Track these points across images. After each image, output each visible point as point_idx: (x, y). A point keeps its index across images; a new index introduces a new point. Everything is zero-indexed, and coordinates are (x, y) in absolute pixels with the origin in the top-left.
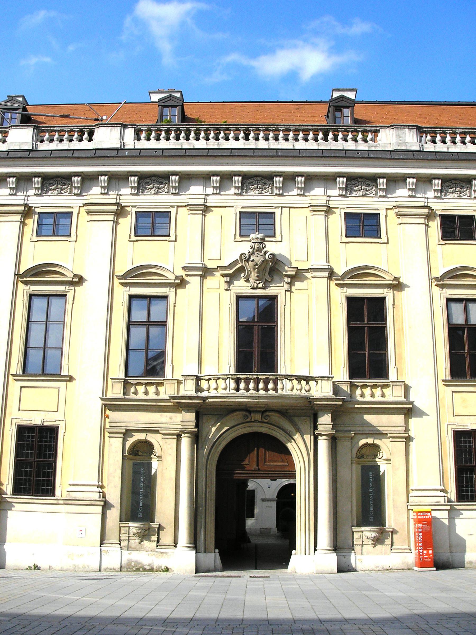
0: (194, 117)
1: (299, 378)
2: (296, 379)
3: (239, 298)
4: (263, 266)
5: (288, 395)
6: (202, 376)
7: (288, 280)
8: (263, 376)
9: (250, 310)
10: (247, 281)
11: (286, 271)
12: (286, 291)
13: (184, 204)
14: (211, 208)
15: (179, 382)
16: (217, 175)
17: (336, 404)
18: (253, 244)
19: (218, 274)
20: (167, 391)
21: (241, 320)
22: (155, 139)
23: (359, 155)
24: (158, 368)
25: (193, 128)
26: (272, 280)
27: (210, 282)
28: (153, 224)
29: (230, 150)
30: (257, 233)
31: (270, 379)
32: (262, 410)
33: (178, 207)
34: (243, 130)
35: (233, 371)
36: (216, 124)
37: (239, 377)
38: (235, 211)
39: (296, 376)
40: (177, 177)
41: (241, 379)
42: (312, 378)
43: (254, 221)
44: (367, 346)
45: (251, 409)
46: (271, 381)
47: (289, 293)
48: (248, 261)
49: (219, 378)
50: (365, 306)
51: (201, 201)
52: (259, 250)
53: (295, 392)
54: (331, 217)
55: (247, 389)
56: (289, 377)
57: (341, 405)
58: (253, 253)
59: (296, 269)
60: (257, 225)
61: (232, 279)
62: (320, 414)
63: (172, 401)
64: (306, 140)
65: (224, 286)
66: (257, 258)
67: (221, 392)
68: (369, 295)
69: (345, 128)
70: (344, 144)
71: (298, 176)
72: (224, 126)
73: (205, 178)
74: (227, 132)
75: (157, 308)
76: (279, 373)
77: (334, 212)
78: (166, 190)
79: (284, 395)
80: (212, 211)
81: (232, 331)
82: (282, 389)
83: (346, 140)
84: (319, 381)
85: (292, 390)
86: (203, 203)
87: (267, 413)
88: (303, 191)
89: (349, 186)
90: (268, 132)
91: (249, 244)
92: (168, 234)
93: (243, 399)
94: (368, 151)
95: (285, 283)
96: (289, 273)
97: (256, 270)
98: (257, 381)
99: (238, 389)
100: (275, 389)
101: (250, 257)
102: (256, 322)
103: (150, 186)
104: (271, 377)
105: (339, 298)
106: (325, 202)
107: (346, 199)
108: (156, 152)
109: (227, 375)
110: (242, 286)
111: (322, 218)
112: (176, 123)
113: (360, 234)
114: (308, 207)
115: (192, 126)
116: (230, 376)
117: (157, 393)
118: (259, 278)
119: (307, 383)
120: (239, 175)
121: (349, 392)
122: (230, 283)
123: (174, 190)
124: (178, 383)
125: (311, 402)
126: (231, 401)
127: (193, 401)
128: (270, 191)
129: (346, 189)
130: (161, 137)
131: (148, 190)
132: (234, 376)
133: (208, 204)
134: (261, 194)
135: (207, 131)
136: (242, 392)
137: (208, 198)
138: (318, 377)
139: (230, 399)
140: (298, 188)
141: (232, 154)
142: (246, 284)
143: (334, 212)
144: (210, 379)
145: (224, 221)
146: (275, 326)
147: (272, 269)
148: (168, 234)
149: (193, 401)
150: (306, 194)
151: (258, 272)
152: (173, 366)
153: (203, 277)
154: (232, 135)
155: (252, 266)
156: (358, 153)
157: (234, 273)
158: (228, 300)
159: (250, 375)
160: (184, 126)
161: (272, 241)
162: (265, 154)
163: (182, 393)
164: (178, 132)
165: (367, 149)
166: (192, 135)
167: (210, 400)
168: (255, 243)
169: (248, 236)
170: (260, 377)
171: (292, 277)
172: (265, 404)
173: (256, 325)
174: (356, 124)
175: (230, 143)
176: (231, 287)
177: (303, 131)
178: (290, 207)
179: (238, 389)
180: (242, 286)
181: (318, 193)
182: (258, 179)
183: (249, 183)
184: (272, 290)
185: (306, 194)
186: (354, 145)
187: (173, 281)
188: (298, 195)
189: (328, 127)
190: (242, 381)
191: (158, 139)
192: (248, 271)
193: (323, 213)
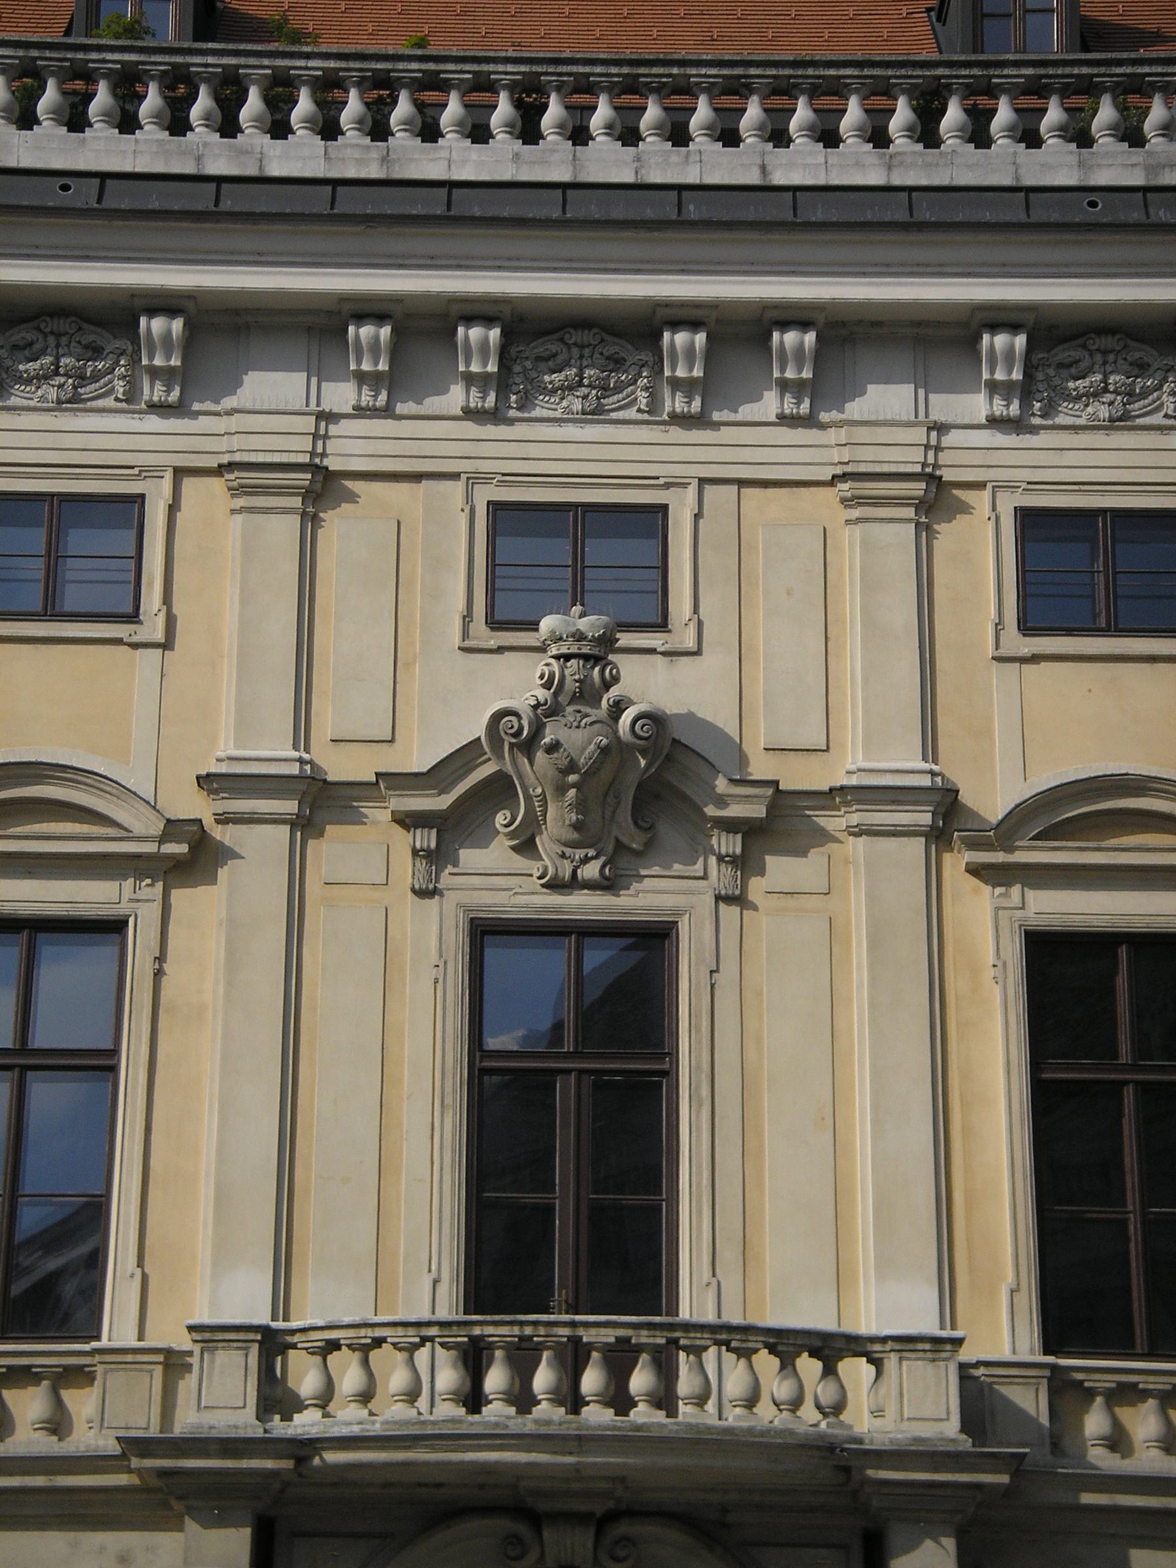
0: (261, 13)
1: (786, 1344)
2: (772, 1349)
3: (485, 932)
4: (606, 775)
5: (729, 1430)
6: (293, 1332)
7: (731, 844)
8: (601, 1330)
9: (539, 990)
10: (526, 847)
11: (721, 801)
12: (718, 898)
13: (212, 462)
14: (349, 484)
15: (174, 1363)
16: (380, 318)
17: (978, 1486)
18: (556, 666)
19: (379, 814)
20: (98, 1418)
21: (493, 1043)
22: (60, 123)
23: (1096, 214)
24: (69, 1288)
25: (257, 69)
26: (649, 844)
27: (341, 852)
28: (54, 557)
29: (444, 191)
30: (577, 609)
31: (639, 1349)
32: (599, 1508)
33: (180, 473)
34: (512, 87)
35: (448, 1306)
36: (372, 50)
37: (482, 1337)
38: (469, 497)
39: (769, 1331)
40: (177, 325)
41: (491, 1347)
42: (856, 1345)
43: (561, 550)
44: (1132, 1181)
45: (542, 1506)
46: (644, 1358)
47: (735, 910)
49: (378, 1342)
50: (1122, 982)
51: (297, 449)
52: (587, 694)
53: (766, 1413)
54: (948, 534)
55: (523, 1399)
56: (737, 1338)
57: (1007, 1492)
58: (554, 711)
59: (770, 791)
60: (579, 567)
62: (896, 1534)
63: (135, 1462)
64: (829, 138)
65: (406, 870)
66: (577, 737)
67: (392, 1413)
68: (1139, 925)
69: (1029, 71)
70: (1021, 160)
71: (784, 325)
72: (414, 66)
73: (317, 330)
74: (430, 96)
75: (64, 973)
76: (685, 1313)
77: (965, 508)
78: (120, 388)
79: (709, 1429)
80: (352, 497)
81: (448, 1100)
82: (701, 1400)
83: (1032, 139)
84: (891, 1362)
85: (751, 1401)
86: (305, 459)
87: (623, 1528)
88: (807, 401)
89: (1040, 376)
90: (634, 100)
91: (542, 665)
92: (130, 609)
93: (501, 1448)
94: (1145, 190)
95: (713, 860)
96: (734, 811)
97: (572, 792)
98: (574, 1358)
99: (474, 1399)
100: (665, 1400)
101: (538, 730)
102: (568, 1056)
103: (36, 365)
104: (643, 1337)
105: (987, 930)
106: (918, 455)
107: (1028, 440)
108: (65, 188)
109: (418, 1325)
111: (283, 530)
112: (170, 37)
113: (1095, 616)
115: (252, 61)
116: (433, 1331)
117: (58, 1424)
118: (584, 834)
119: (830, 1371)
120: (488, 320)
121: (1045, 1420)
122: (437, 858)
123: (159, 386)
124: (167, 1366)
125: (847, 1470)
126: (438, 1464)
127: (245, 1464)
128: (643, 399)
129: (1026, 391)
130: (94, 107)
131: (28, 382)
132: (455, 1330)
133: (333, 464)
134: (595, 414)
135: (328, 91)
136: (496, 1411)
137: (333, 430)
138: (884, 1340)
139: (434, 1449)
140: (784, 385)
141: (451, 215)
142: (520, 863)
143: (965, 508)
144: (333, 1346)
145: (408, 552)
146: (664, 1073)
147: (653, 787)
148: (130, 609)
149: (245, 1464)
150: (824, 417)
151: (580, 805)
152: (145, 1279)
153: (306, 826)
154: (453, 110)
155: (552, 773)
156: (1093, 204)
157: (456, 809)
158: (430, 939)
159: (535, 1324)
160: (210, 60)
161: (652, 651)
162: (617, 214)
163: (188, 1420)
164: (182, 90)
165: (1137, 179)
166: (253, 105)
167: (333, 1457)
168: (567, 657)
169: (533, 626)
170: (587, 1336)
171: (748, 829)
172: (614, 1479)
173: (568, 1071)
174: (1086, 48)
175: (444, 154)
176: (446, 880)
177: (814, 93)
178: (742, 483)
179: (474, 1399)
180: (499, 876)
181: (885, 409)
182: (585, 336)
183: (539, 359)
184: (648, 896)
185: (824, 417)
186: (1074, 159)
187: (150, 848)
188: (785, 420)
189: (940, 71)
190: (499, 1353)
191: (75, 120)
192: (528, 798)
193: (910, 512)
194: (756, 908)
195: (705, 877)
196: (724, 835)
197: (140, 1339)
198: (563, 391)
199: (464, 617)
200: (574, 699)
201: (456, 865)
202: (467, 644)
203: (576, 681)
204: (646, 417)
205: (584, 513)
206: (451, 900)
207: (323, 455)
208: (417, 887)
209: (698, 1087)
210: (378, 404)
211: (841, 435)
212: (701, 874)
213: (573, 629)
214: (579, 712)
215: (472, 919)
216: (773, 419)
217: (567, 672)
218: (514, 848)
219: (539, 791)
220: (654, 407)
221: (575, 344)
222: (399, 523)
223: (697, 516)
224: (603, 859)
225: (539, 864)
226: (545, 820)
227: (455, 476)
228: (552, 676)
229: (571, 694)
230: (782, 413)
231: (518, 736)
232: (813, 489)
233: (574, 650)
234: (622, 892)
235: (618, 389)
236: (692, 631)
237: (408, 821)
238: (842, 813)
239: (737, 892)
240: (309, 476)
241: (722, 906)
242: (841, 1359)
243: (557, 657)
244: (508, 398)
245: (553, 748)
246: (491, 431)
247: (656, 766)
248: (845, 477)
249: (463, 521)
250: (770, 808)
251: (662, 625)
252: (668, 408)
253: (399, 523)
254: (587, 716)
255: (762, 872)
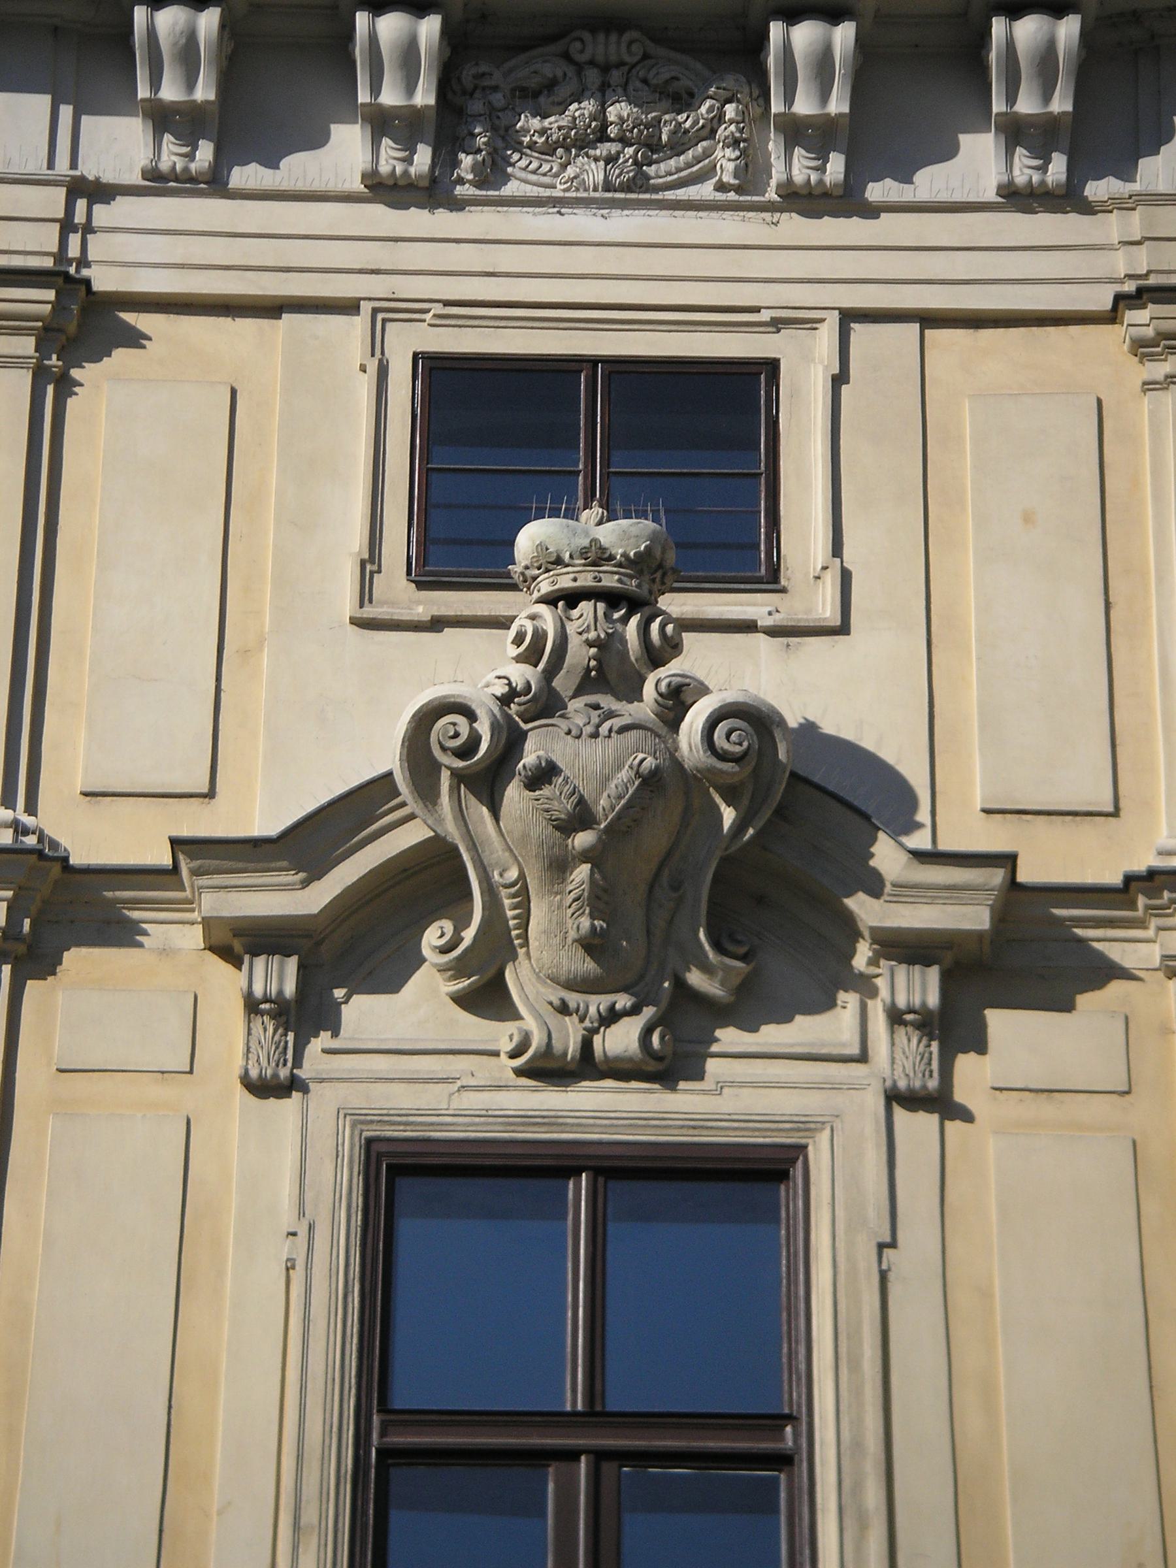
3: (403, 1177)
4: (655, 837)
7: (923, 987)
10: (487, 997)
12: (895, 1098)
14: (129, 317)
18: (548, 618)
19: (173, 937)
30: (596, 511)
38: (376, 343)
47: (927, 1122)
48: (487, 782)
52: (611, 675)
58: (546, 705)
59: (997, 876)
61: (324, 967)
66: (593, 756)
80: (135, 339)
81: (310, 1515)
97: (582, 872)
101: (511, 742)
110: (422, 1053)
114: (1112, 317)
122: (304, 1015)
134: (633, 190)
137: (103, 214)
146: (784, 1461)
147: (751, 869)
151: (600, 899)
155: (540, 829)
157: (342, 924)
158: (275, 1193)
161: (748, 627)
168: (572, 598)
173: (572, 1456)
178: (929, 320)
180: (422, 1053)
184: (745, 1086)
188: (1016, 198)
194: (966, 1116)
195: (863, 1058)
196: (901, 971)
197: (49, 168)
198: (568, 150)
199: (363, 564)
200: (586, 685)
201: (336, 1034)
202: (369, 612)
203: (590, 644)
204: (732, 196)
205: (607, 377)
206: (325, 1102)
207: (83, 262)
208: (254, 1073)
209: (858, 1486)
210: (193, 167)
211: (1135, 223)
212: (855, 1050)
213: (585, 542)
214: (596, 707)
215: (370, 1142)
216: (991, 196)
217: (571, 628)
218: (460, 1000)
219: (513, 874)
220: (751, 174)
221: (592, 63)
222: (234, 392)
223: (840, 380)
224: (648, 1012)
225: (511, 1027)
226: (525, 936)
227: (349, 307)
228: (539, 636)
229: (580, 672)
230: (1011, 183)
231: (466, 757)
232: (1074, 330)
233: (586, 580)
234: (682, 1085)
235: (678, 146)
236: (829, 589)
237: (238, 942)
238: (1150, 933)
239: (933, 1084)
240: (50, 295)
241: (899, 1113)
242: (965, 1051)
243: (551, 600)
244: (456, 164)
245: (544, 774)
246: (417, 220)
247: (761, 822)
248: (1143, 295)
249: (365, 387)
250: (1001, 916)
251: (771, 579)
252: (778, 174)
253: (234, 392)
254: (611, 715)
255: (980, 1046)
